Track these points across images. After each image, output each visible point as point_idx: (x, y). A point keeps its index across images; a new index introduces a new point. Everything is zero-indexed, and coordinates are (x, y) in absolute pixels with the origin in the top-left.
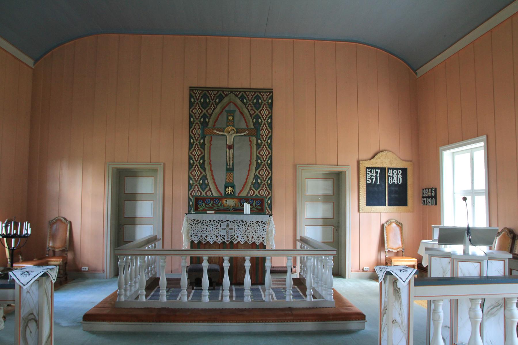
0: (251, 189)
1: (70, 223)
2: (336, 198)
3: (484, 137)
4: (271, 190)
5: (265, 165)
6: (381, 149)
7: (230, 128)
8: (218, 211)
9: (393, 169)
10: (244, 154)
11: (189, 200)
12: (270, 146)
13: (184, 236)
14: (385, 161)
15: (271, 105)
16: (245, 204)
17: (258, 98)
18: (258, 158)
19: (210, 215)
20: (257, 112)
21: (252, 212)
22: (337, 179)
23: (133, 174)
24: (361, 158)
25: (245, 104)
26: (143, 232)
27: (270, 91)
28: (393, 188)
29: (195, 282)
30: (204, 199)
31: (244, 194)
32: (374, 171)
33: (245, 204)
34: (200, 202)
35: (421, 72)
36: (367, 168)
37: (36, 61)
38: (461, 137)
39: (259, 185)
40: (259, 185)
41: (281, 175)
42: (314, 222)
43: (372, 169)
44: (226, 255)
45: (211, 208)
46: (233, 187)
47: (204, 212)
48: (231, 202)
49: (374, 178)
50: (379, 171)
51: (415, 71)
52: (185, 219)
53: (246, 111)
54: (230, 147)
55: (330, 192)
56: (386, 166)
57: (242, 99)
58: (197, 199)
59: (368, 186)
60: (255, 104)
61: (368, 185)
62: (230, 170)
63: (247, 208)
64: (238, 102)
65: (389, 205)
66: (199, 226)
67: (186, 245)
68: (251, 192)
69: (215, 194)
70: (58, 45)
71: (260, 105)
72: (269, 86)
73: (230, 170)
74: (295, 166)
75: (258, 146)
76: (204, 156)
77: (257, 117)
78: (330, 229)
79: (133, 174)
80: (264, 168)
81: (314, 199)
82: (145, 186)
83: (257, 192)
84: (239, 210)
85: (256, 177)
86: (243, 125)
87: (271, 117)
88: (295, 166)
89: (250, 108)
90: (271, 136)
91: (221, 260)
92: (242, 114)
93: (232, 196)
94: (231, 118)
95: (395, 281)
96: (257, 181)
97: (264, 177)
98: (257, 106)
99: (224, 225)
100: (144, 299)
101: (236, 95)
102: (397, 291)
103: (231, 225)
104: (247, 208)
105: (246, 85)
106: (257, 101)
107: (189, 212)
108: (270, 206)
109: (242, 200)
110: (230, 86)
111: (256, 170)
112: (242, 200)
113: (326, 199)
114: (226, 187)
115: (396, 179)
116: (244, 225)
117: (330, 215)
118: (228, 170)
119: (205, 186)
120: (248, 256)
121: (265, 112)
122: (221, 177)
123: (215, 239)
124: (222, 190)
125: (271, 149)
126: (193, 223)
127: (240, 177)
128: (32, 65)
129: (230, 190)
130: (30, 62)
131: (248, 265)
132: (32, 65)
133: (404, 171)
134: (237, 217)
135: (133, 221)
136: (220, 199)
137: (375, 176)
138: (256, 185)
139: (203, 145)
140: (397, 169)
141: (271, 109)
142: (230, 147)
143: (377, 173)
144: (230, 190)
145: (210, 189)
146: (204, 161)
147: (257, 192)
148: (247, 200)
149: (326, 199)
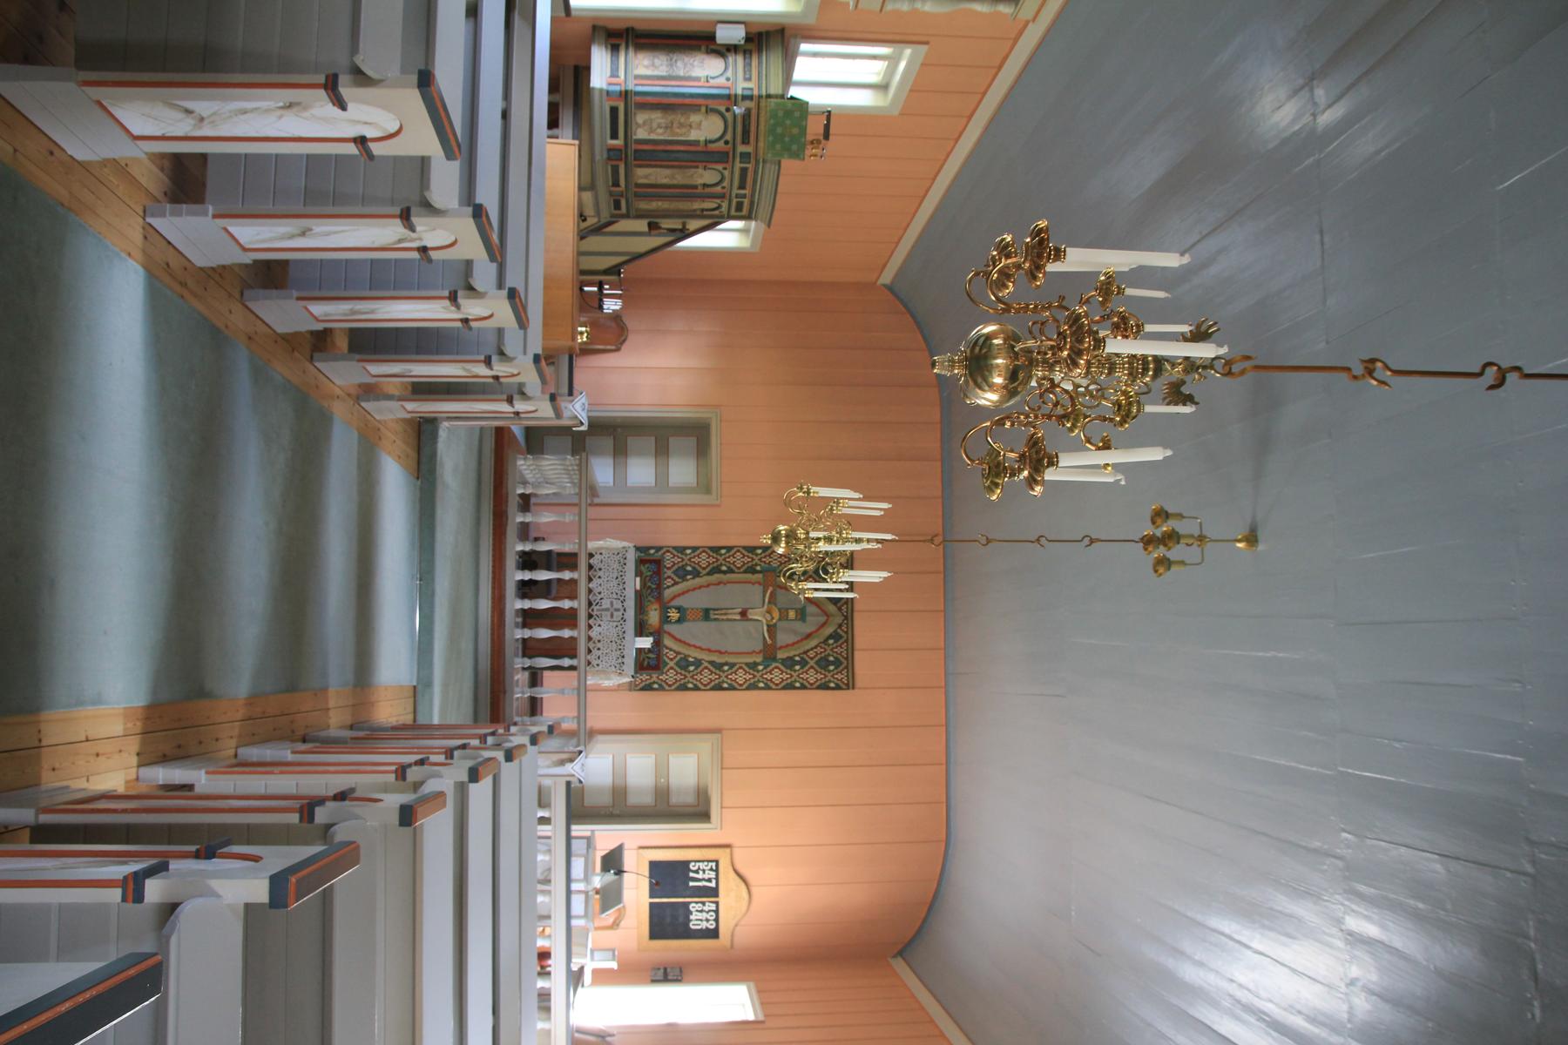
0: (678, 653)
1: (618, 350)
2: (664, 808)
3: (761, 1017)
4: (678, 689)
5: (718, 676)
6: (754, 890)
7: (776, 615)
8: (640, 597)
9: (717, 912)
10: (743, 639)
11: (658, 549)
12: (753, 687)
13: (601, 543)
14: (731, 899)
15: (824, 687)
16: (651, 639)
17: (837, 663)
18: (732, 665)
19: (634, 583)
20: (812, 663)
21: (639, 651)
22: (699, 812)
23: (702, 451)
24: (737, 852)
25: (825, 641)
26: (603, 471)
27: (850, 685)
28: (681, 911)
29: (529, 561)
30: (658, 573)
31: (667, 642)
32: (713, 875)
33: (651, 639)
34: (653, 567)
35: (899, 965)
36: (717, 862)
37: (889, 288)
38: (763, 997)
39: (685, 668)
40: (685, 668)
41: (703, 706)
42: (619, 770)
43: (717, 871)
44: (579, 604)
45: (643, 584)
46: (679, 621)
47: (638, 573)
48: (654, 617)
49: (700, 876)
50: (713, 884)
51: (900, 953)
52: (625, 544)
53: (813, 643)
54: (744, 614)
55: (674, 800)
56: (721, 899)
57: (835, 636)
58: (658, 563)
59: (685, 865)
60: (825, 659)
61: (685, 864)
62: (706, 614)
63: (646, 643)
64: (829, 630)
65: (651, 905)
66: (616, 566)
67: (593, 545)
68: (671, 655)
69: (668, 593)
70: (916, 322)
71: (825, 668)
72: (859, 683)
73: (706, 614)
74: (718, 731)
75: (753, 666)
76: (732, 571)
77: (803, 663)
78: (606, 800)
79: (702, 451)
80: (713, 677)
81: (661, 768)
82: (682, 471)
83: (672, 664)
84: (641, 630)
85: (698, 663)
86: (783, 638)
87: (803, 687)
88: (718, 731)
89: (819, 650)
90: (769, 688)
91: (573, 596)
92: (809, 636)
93: (665, 619)
94: (792, 614)
95: (572, 760)
96: (692, 664)
97: (698, 677)
98: (823, 663)
99: (617, 604)
100: (520, 491)
101: (840, 626)
102: (562, 763)
103: (617, 615)
104: (646, 643)
105: (860, 641)
106: (832, 663)
107: (638, 549)
108: (648, 688)
109: (658, 635)
110: (856, 615)
111: (711, 663)
112: (658, 635)
113: (662, 793)
114: (679, 609)
115: (699, 917)
116: (616, 639)
117: (633, 800)
118: (707, 611)
119: (682, 574)
120: (579, 633)
121: (812, 676)
122: (695, 601)
123: (596, 591)
124: (675, 603)
125: (748, 689)
126: (621, 555)
127: (695, 632)
128: (881, 281)
129: (674, 615)
130: (887, 277)
131: (566, 633)
132: (881, 281)
133: (713, 934)
134: (630, 626)
135: (620, 452)
136: (659, 598)
137: (702, 876)
138: (684, 664)
139: (751, 570)
140: (717, 920)
141: (819, 688)
142: (744, 614)
143: (709, 880)
144: (674, 615)
145: (676, 583)
146: (725, 572)
147: (672, 664)
148: (657, 643)
149: (662, 793)
